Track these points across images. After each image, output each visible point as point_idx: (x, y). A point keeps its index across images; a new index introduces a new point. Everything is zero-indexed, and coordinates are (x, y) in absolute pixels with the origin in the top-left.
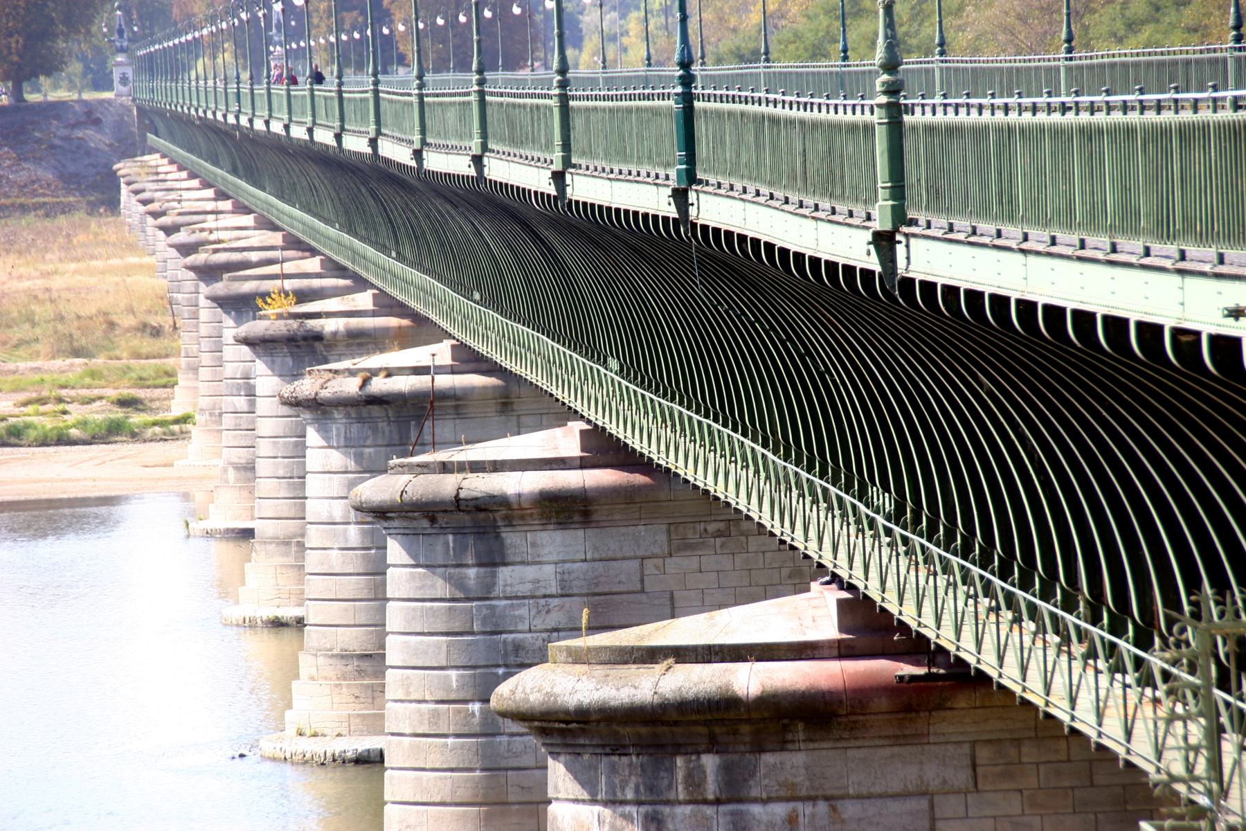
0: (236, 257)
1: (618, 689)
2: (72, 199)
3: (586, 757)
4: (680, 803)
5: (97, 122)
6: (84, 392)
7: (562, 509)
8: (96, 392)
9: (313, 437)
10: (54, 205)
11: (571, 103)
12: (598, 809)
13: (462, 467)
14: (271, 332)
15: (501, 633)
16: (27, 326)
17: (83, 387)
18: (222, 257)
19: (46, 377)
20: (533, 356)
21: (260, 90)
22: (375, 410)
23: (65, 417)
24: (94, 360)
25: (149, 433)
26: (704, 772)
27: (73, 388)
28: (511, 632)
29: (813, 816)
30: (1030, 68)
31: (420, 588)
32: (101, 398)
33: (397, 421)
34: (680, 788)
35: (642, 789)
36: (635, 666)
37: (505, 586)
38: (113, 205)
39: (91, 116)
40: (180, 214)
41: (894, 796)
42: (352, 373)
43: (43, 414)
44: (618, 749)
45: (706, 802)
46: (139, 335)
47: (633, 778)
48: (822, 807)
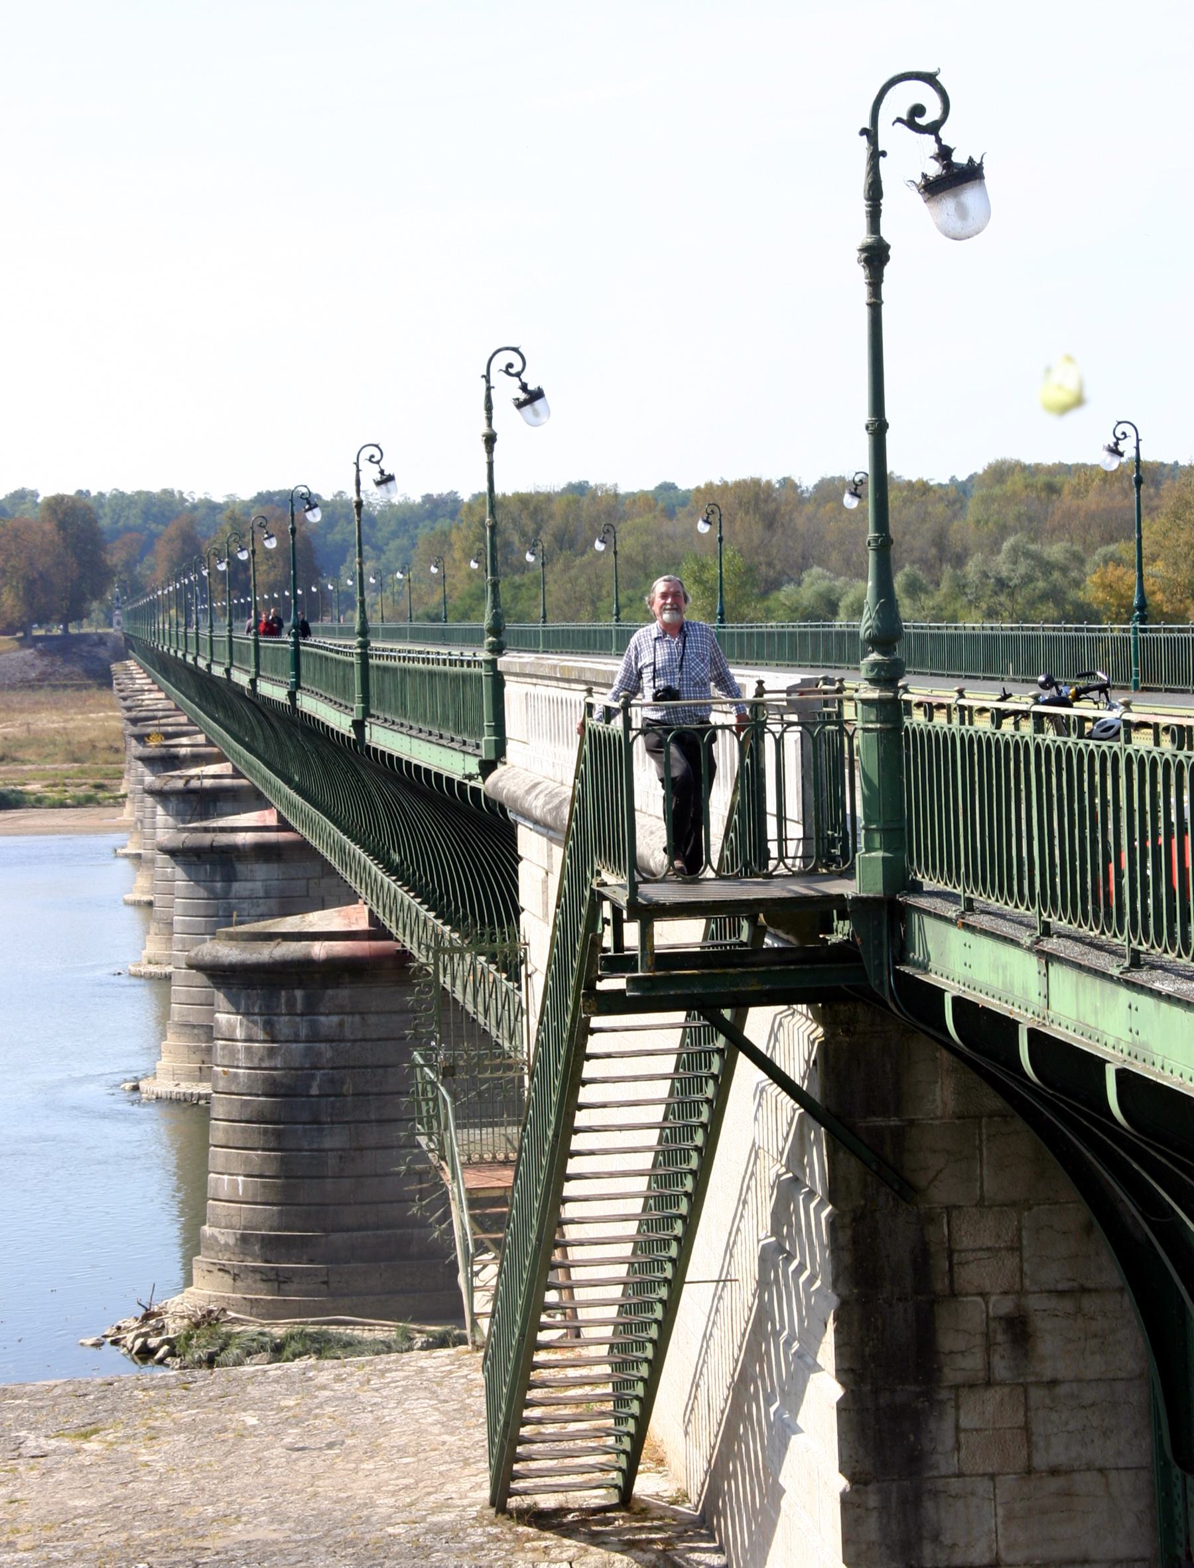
0: (150, 714)
5: (105, 644)
7: (264, 852)
9: (160, 810)
12: (239, 1017)
13: (215, 830)
18: (144, 714)
20: (262, 776)
21: (192, 631)
22: (192, 797)
25: (106, 802)
29: (352, 1022)
33: (201, 803)
38: (109, 685)
39: (101, 640)
41: (395, 1012)
42: (180, 777)
44: (249, 986)
45: (296, 1015)
48: (357, 1018)
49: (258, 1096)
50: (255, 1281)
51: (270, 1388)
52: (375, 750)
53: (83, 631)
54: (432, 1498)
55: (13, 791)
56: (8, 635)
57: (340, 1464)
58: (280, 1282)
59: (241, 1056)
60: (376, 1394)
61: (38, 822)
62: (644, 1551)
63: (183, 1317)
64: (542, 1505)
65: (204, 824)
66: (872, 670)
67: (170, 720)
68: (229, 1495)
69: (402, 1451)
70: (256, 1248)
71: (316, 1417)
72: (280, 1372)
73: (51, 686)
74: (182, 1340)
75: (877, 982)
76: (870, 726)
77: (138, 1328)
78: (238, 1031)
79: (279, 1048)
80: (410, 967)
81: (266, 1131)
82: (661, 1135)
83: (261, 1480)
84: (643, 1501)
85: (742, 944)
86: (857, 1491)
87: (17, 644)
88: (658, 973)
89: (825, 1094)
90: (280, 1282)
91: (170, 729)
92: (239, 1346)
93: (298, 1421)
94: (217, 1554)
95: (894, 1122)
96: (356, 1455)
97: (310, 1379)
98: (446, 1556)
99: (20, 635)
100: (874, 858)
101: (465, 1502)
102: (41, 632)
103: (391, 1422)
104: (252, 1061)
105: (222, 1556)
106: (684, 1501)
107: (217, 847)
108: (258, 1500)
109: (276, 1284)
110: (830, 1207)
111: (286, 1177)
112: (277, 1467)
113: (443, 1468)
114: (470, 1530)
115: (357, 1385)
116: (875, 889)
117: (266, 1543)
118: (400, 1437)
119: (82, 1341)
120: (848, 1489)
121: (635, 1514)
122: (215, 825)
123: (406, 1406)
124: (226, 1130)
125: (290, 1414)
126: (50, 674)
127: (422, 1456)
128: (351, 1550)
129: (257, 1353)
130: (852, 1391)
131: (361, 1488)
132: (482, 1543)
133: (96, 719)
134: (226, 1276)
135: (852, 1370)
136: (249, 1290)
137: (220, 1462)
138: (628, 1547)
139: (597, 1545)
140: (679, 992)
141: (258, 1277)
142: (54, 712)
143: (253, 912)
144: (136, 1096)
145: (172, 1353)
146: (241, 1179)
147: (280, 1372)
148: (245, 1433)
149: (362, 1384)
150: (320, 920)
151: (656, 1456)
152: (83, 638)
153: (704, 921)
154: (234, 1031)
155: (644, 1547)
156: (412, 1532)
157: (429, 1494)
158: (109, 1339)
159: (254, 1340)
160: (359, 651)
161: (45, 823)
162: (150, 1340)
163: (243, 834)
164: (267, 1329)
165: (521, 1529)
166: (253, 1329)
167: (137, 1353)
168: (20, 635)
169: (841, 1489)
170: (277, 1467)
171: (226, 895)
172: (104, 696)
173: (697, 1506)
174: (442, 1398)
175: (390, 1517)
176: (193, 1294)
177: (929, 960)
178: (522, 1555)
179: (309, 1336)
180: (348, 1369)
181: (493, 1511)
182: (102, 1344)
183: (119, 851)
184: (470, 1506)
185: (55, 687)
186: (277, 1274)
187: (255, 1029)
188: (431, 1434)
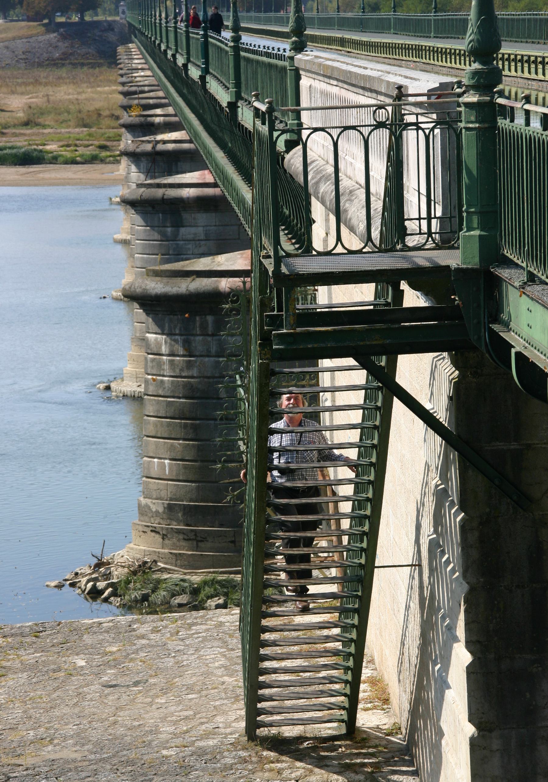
1: (172, 288)
2: (102, 61)
3: (160, 315)
4: (198, 335)
5: (113, 30)
6: (86, 143)
7: (205, 204)
8: (91, 142)
9: (133, 168)
10: (95, 63)
11: (169, 28)
12: (164, 337)
14: (133, 122)
15: (181, 255)
16: (66, 114)
17: (85, 140)
18: (134, 89)
19: (72, 136)
23: (76, 152)
24: (92, 129)
26: (208, 323)
27: (82, 140)
28: (185, 255)
30: (537, 19)
31: (148, 235)
32: (92, 145)
34: (198, 329)
35: (182, 329)
36: (180, 278)
37: (183, 235)
39: (110, 27)
40: (128, 69)
42: (149, 142)
43: (68, 151)
45: (208, 335)
46: (110, 119)
47: (179, 325)
49: (179, 398)
50: (179, 540)
51: (101, 637)
52: (243, 126)
53: (95, 19)
54: (203, 727)
55: (35, 150)
56: (37, 21)
57: (140, 698)
58: (198, 541)
59: (166, 367)
60: (181, 643)
61: (53, 175)
62: (357, 773)
63: (124, 567)
64: (287, 734)
65: (157, 181)
66: (473, 78)
67: (152, 94)
68: (49, 722)
69: (190, 689)
70: (180, 515)
71: (131, 660)
72: (111, 624)
73: (71, 63)
74: (123, 584)
75: (476, 337)
76: (471, 125)
77: (91, 574)
78: (163, 347)
79: (195, 361)
80: (223, 309)
81: (186, 426)
82: (359, 452)
83: (77, 710)
84: (365, 732)
85: (388, 304)
86: (483, 736)
87: (43, 29)
88: (299, 330)
89: (458, 425)
90: (198, 541)
91: (151, 101)
92: (165, 590)
93: (116, 663)
94: (27, 769)
95: (514, 446)
96: (154, 691)
97: (134, 630)
98: (202, 774)
99: (46, 21)
100: (472, 236)
101: (228, 730)
102: (62, 20)
103: (188, 665)
104: (174, 372)
105: (29, 772)
106: (397, 733)
107: (166, 199)
108: (71, 726)
109: (195, 543)
110: (463, 514)
111: (202, 461)
112: (91, 700)
113: (217, 703)
114: (226, 754)
115: (168, 635)
116: (474, 262)
117: (67, 762)
118: (191, 677)
119: (48, 583)
120: (476, 735)
121: (356, 742)
122: (165, 182)
123: (201, 653)
124: (155, 425)
125: (111, 658)
126: (71, 54)
127: (204, 693)
128: (130, 768)
129: (179, 595)
130: (479, 658)
131: (151, 718)
132: (232, 765)
133: (101, 93)
134: (157, 536)
135: (479, 642)
136: (174, 547)
137: (49, 695)
138: (344, 769)
139: (320, 767)
140: (316, 346)
141: (181, 537)
142: (71, 86)
143: (196, 251)
144: (108, 394)
145: (114, 594)
146: (167, 462)
147: (111, 624)
148: (74, 672)
149: (172, 635)
150: (227, 260)
151: (383, 697)
152: (95, 24)
153: (374, 284)
154: (160, 348)
155: (357, 769)
156: (181, 755)
157: (202, 723)
158: (69, 582)
159: (177, 585)
160: (232, 44)
161: (58, 176)
162: (98, 584)
163: (187, 189)
164: (187, 577)
165: (265, 753)
166: (177, 576)
167: (88, 594)
168: (46, 21)
169: (470, 734)
170: (91, 700)
171: (175, 238)
172: (113, 74)
173: (405, 737)
174: (230, 647)
175: (167, 742)
176: (132, 549)
177: (511, 321)
178: (260, 774)
179: (219, 582)
180: (164, 623)
181: (246, 738)
182: (63, 586)
183: (113, 199)
184: (231, 734)
185: (74, 65)
186: (196, 535)
187: (176, 346)
188: (215, 675)
